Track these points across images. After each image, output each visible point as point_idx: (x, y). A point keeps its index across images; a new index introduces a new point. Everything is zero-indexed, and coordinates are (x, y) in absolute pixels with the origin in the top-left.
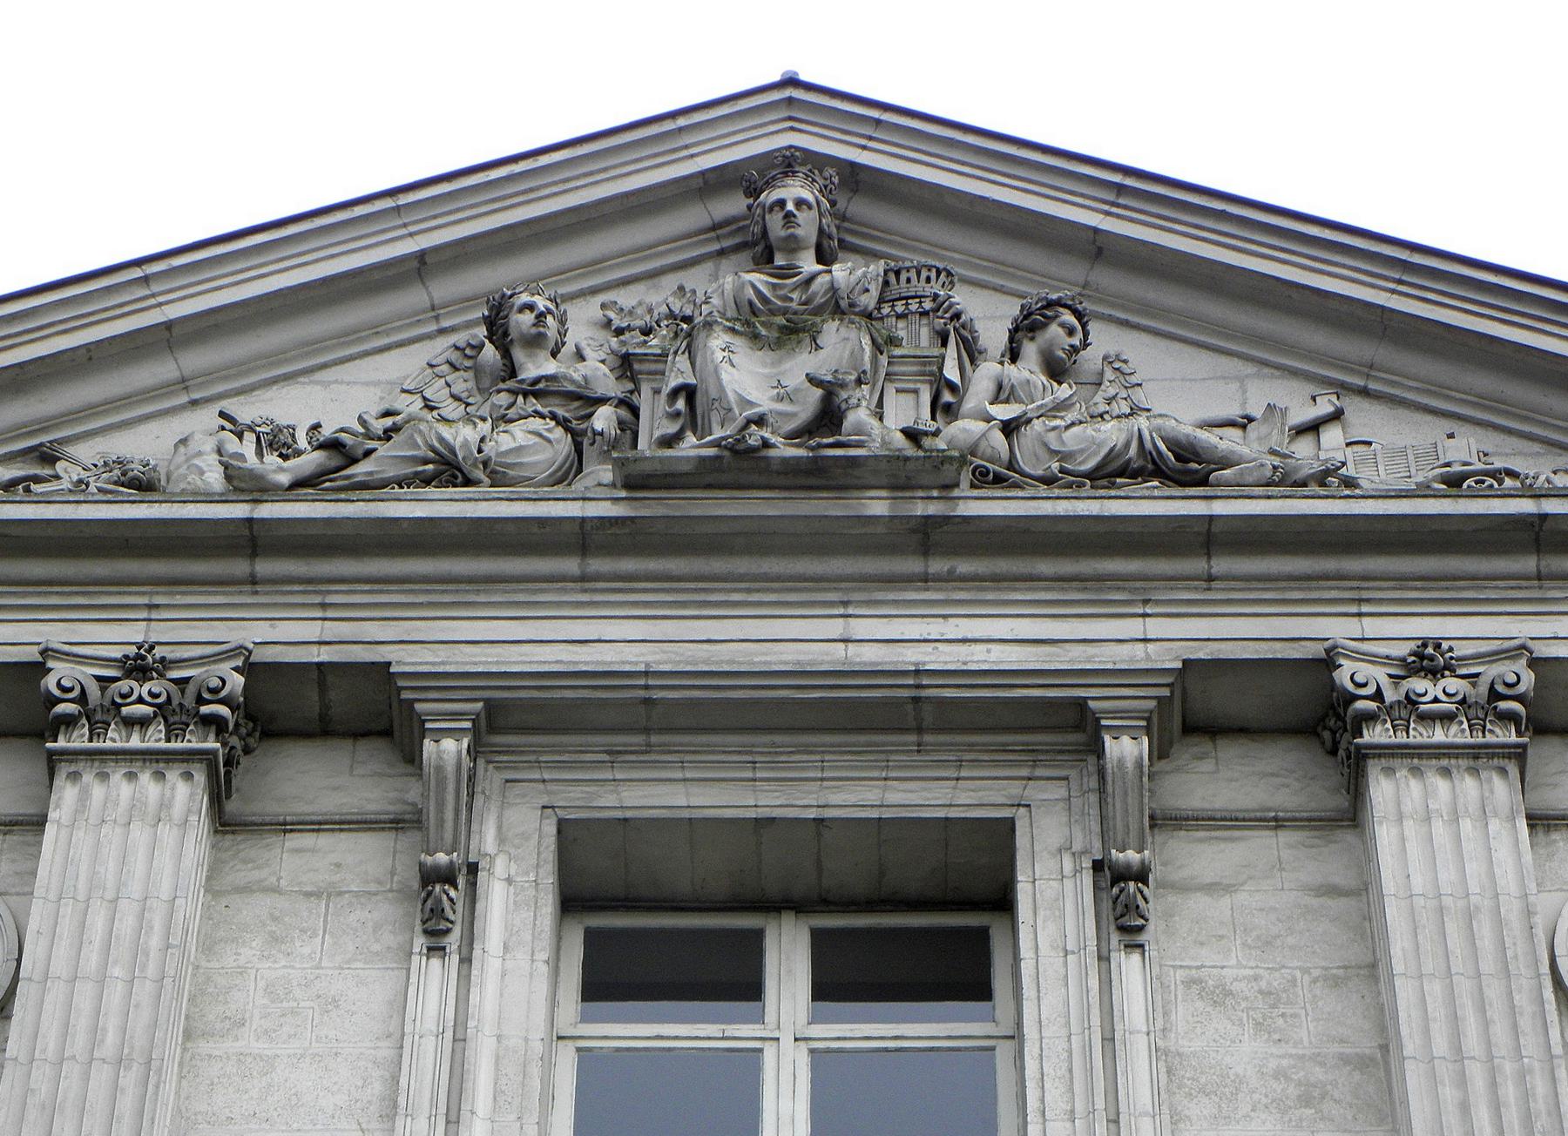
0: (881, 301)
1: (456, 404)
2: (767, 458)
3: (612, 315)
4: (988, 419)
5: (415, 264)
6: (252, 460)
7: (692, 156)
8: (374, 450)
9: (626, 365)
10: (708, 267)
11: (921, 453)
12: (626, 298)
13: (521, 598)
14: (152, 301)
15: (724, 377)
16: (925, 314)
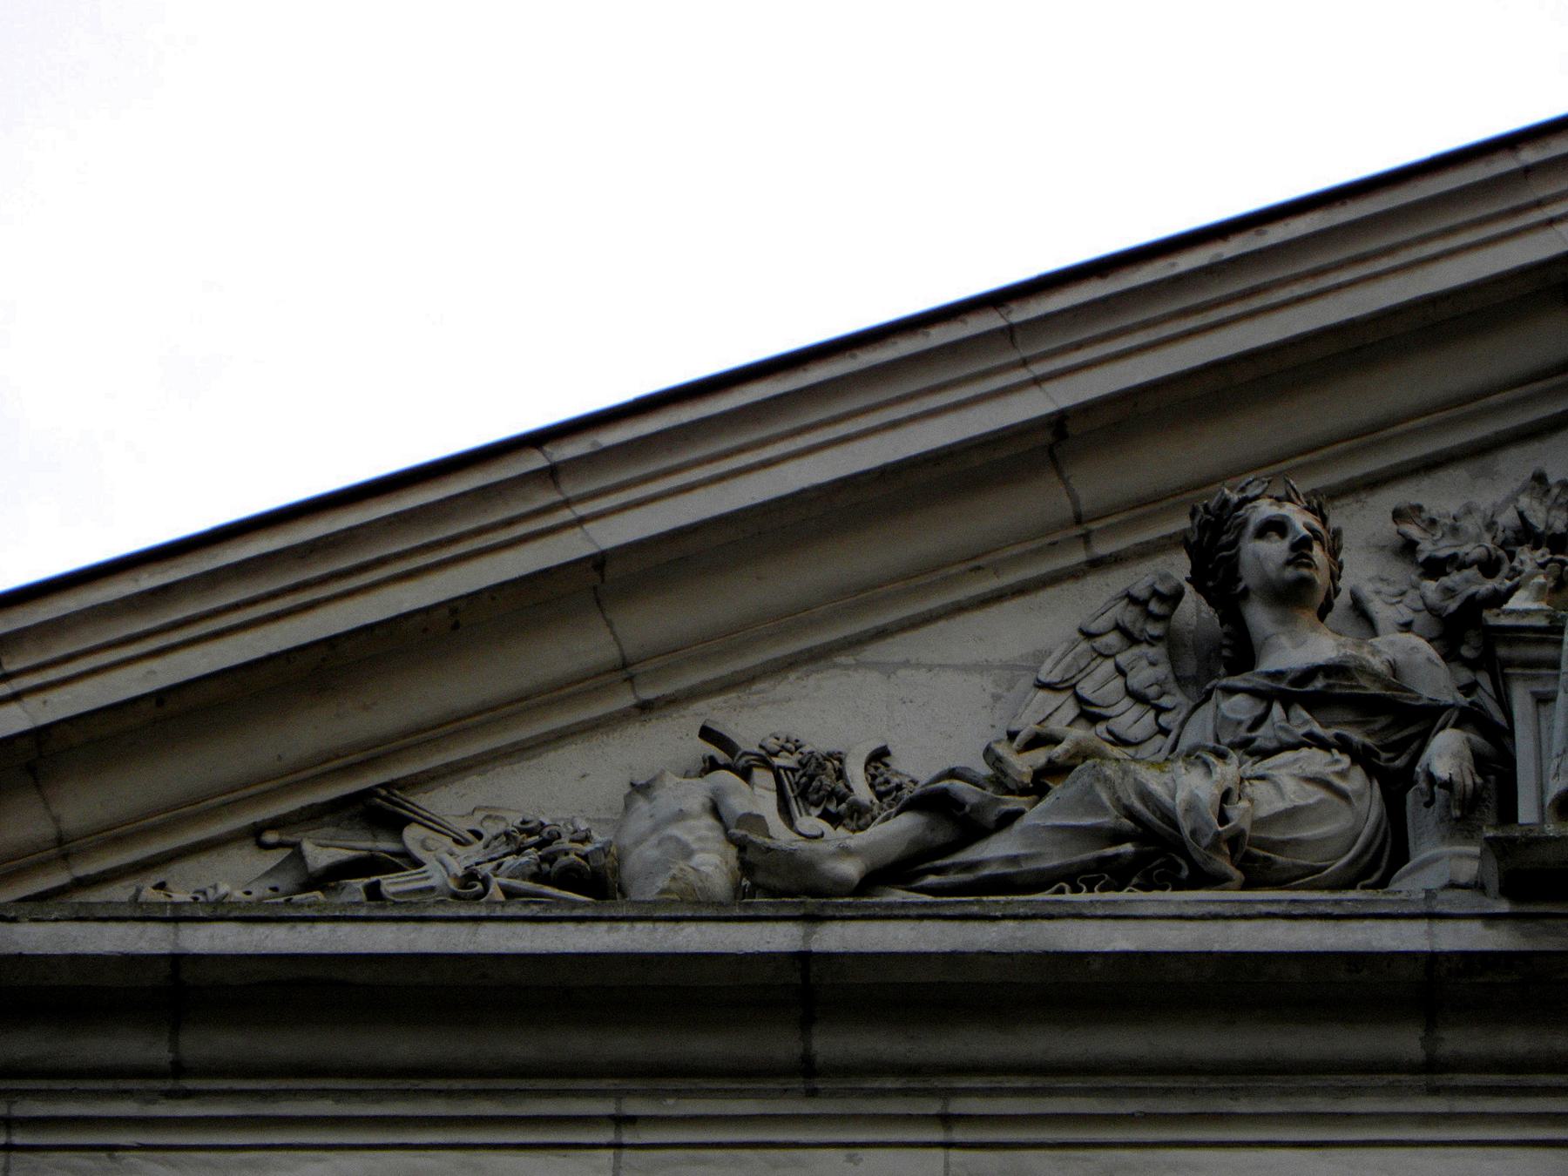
1: (1137, 709)
3: (1413, 531)
5: (1047, 437)
9: (1459, 630)
12: (1441, 496)
13: (1318, 1104)
14: (566, 515)
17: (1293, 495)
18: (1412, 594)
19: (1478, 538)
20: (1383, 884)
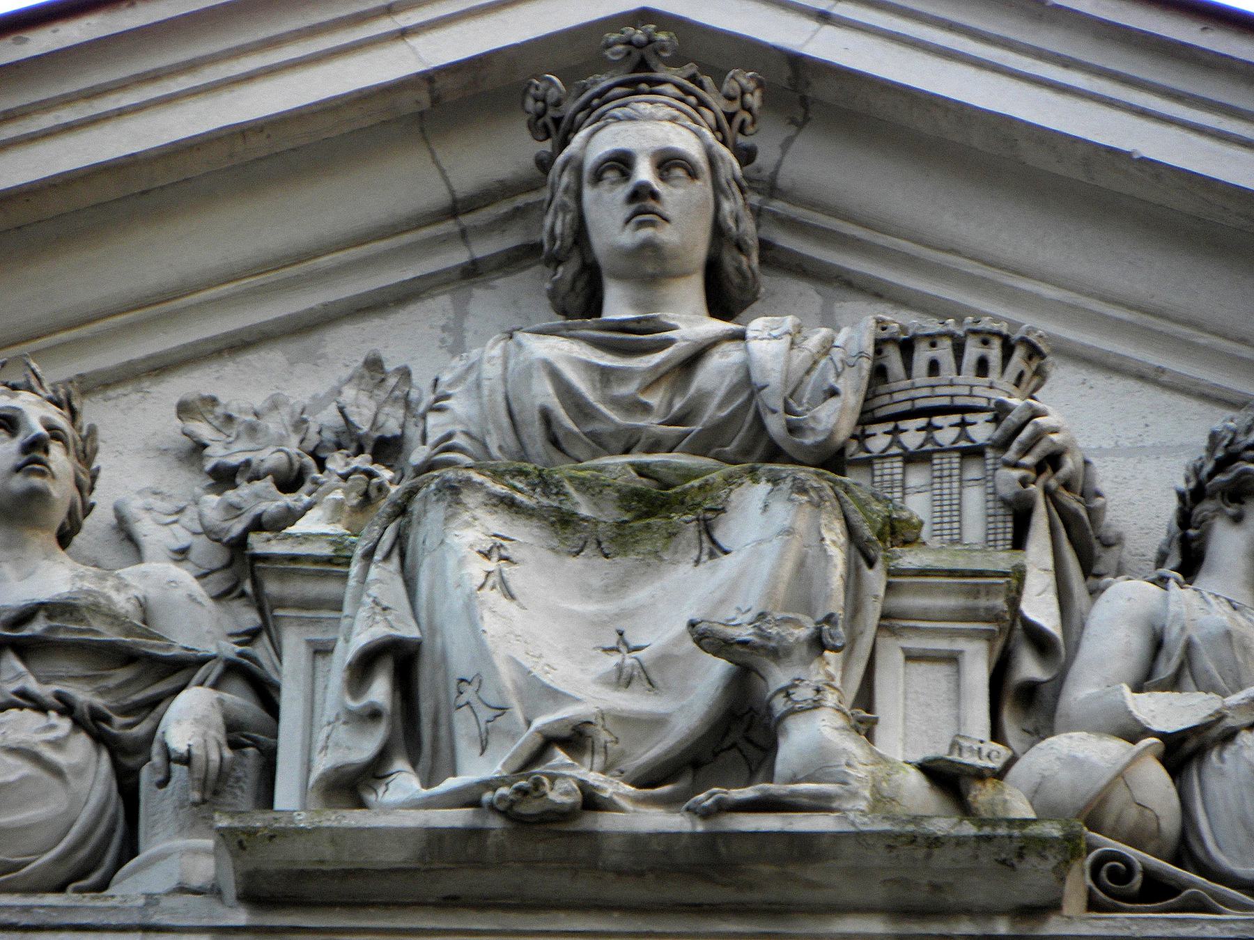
0: (867, 417)
2: (592, 835)
3: (203, 430)
4: (1133, 732)
7: (403, 33)
9: (240, 566)
10: (439, 306)
11: (969, 829)
12: (240, 386)
15: (490, 625)
16: (973, 453)
17: (34, 382)
18: (191, 513)
19: (281, 439)
20: (102, 886)
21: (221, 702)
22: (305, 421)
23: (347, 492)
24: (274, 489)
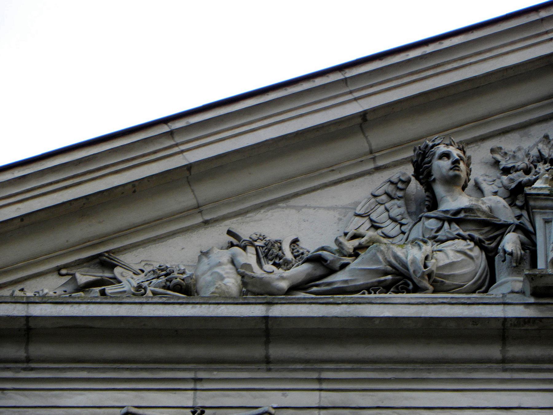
1: (394, 224)
3: (498, 157)
5: (359, 120)
6: (258, 272)
8: (347, 264)
9: (516, 194)
12: (508, 144)
14: (176, 149)
17: (453, 143)
18: (498, 181)
21: (519, 237)
22: (529, 154)
23: (549, 175)
24: (523, 174)
